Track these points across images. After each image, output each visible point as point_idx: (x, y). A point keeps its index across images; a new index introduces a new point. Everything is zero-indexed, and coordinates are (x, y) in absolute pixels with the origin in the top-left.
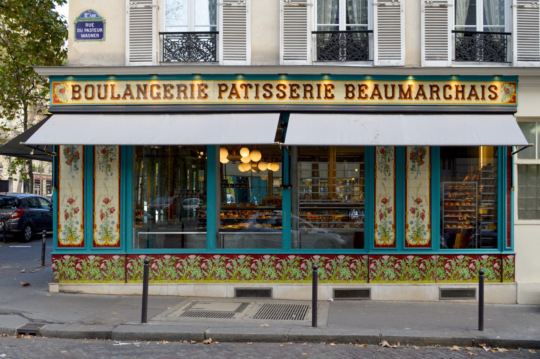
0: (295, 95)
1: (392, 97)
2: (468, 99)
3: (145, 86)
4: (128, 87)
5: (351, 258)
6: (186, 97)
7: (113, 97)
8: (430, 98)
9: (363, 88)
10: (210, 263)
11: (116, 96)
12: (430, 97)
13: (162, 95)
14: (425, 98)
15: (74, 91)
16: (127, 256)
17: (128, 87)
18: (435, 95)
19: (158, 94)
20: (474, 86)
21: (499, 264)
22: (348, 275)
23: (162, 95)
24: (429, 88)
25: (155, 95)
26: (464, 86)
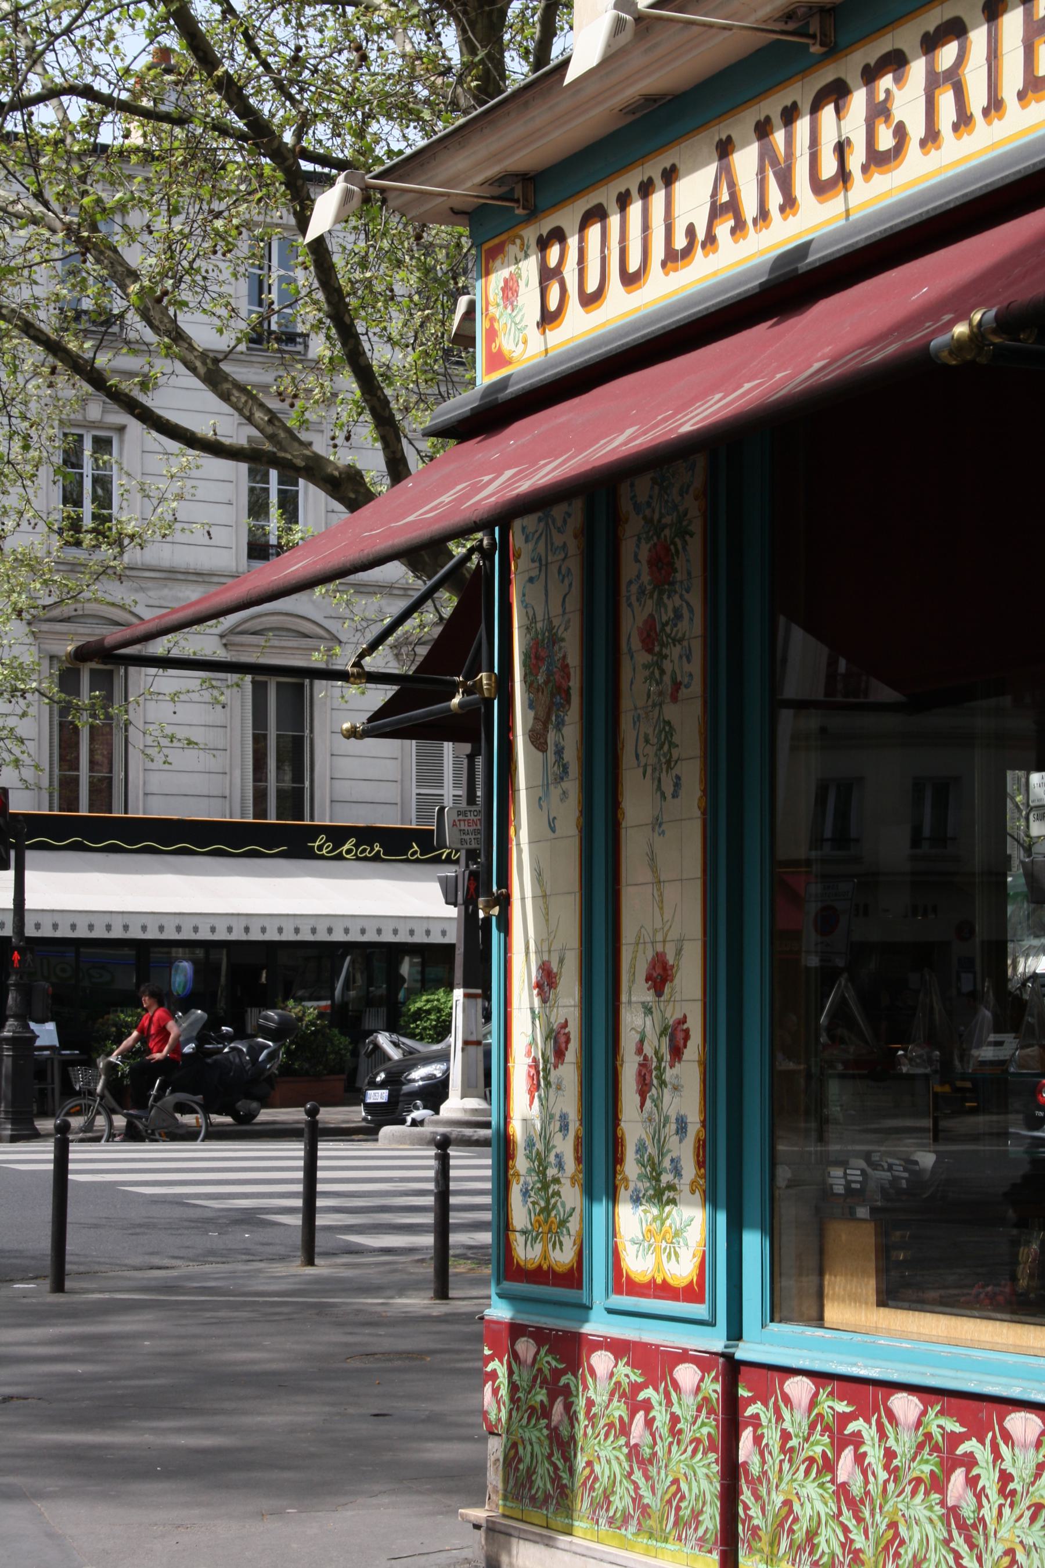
2: (704, 245)
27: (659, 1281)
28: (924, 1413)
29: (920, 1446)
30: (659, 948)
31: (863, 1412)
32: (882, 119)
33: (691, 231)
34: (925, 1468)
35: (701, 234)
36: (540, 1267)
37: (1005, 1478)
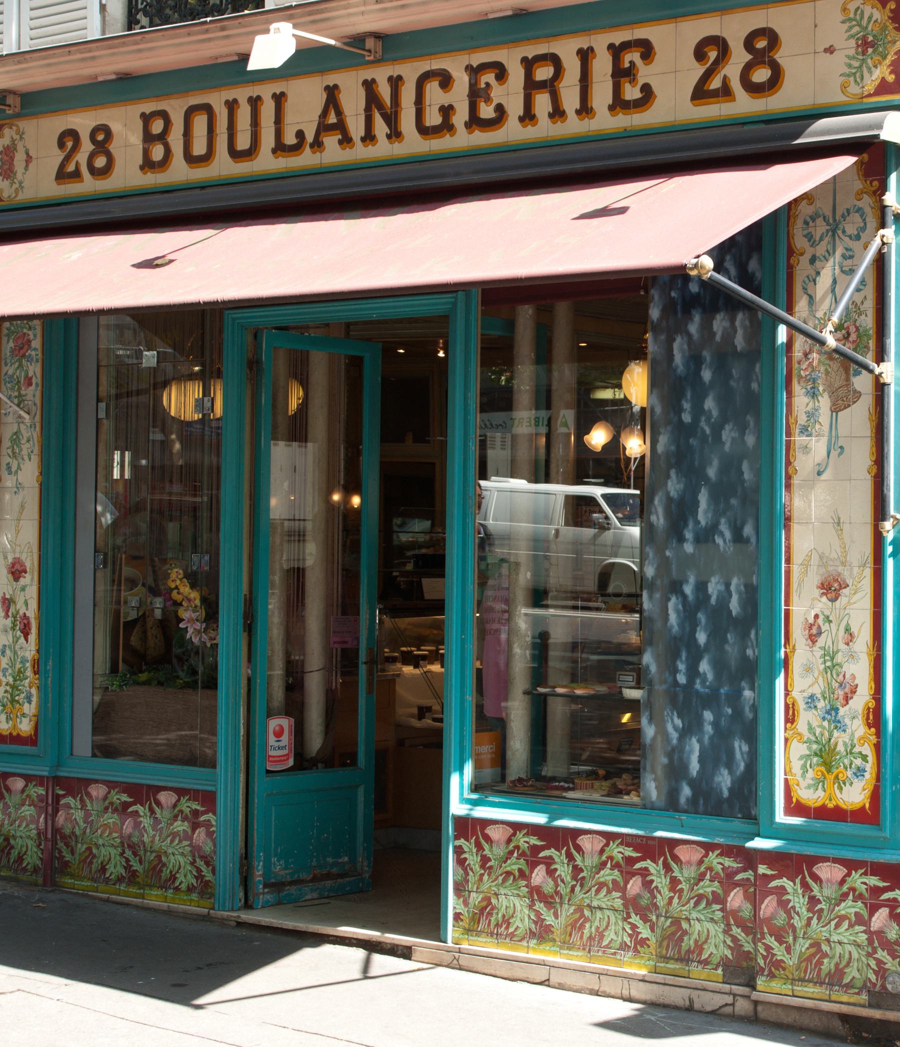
0: (487, 111)
1: (207, 158)
2: (312, 146)
3: (396, 82)
4: (332, 92)
5: (629, 852)
6: (395, 134)
7: (280, 148)
8: (363, 140)
9: (632, 57)
10: (661, 881)
11: (290, 139)
12: (362, 133)
13: (460, 117)
14: (346, 140)
15: (149, 138)
16: (57, 781)
17: (332, 92)
18: (381, 128)
19: (447, 111)
20: (336, 87)
21: (746, 896)
22: (523, 920)
23: (460, 117)
24: (140, 124)
25: (433, 118)
26: (283, 94)
27: (15, 734)
28: (109, 793)
29: (106, 809)
30: (17, 555)
31: (139, 801)
32: (628, 79)
33: (300, 134)
34: (515, 865)
35: (310, 137)
36: (11, 734)
37: (577, 870)
